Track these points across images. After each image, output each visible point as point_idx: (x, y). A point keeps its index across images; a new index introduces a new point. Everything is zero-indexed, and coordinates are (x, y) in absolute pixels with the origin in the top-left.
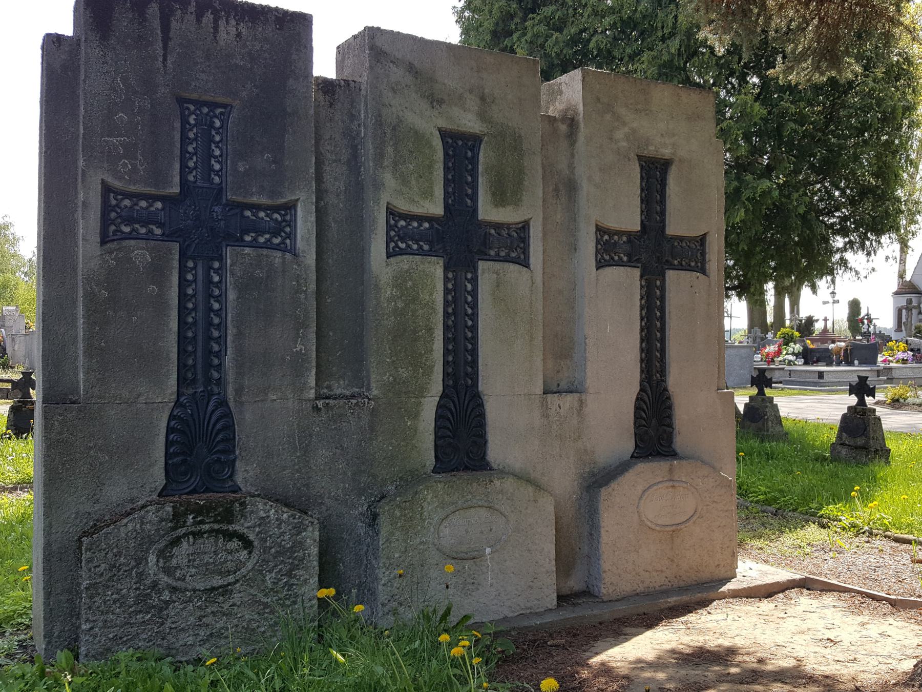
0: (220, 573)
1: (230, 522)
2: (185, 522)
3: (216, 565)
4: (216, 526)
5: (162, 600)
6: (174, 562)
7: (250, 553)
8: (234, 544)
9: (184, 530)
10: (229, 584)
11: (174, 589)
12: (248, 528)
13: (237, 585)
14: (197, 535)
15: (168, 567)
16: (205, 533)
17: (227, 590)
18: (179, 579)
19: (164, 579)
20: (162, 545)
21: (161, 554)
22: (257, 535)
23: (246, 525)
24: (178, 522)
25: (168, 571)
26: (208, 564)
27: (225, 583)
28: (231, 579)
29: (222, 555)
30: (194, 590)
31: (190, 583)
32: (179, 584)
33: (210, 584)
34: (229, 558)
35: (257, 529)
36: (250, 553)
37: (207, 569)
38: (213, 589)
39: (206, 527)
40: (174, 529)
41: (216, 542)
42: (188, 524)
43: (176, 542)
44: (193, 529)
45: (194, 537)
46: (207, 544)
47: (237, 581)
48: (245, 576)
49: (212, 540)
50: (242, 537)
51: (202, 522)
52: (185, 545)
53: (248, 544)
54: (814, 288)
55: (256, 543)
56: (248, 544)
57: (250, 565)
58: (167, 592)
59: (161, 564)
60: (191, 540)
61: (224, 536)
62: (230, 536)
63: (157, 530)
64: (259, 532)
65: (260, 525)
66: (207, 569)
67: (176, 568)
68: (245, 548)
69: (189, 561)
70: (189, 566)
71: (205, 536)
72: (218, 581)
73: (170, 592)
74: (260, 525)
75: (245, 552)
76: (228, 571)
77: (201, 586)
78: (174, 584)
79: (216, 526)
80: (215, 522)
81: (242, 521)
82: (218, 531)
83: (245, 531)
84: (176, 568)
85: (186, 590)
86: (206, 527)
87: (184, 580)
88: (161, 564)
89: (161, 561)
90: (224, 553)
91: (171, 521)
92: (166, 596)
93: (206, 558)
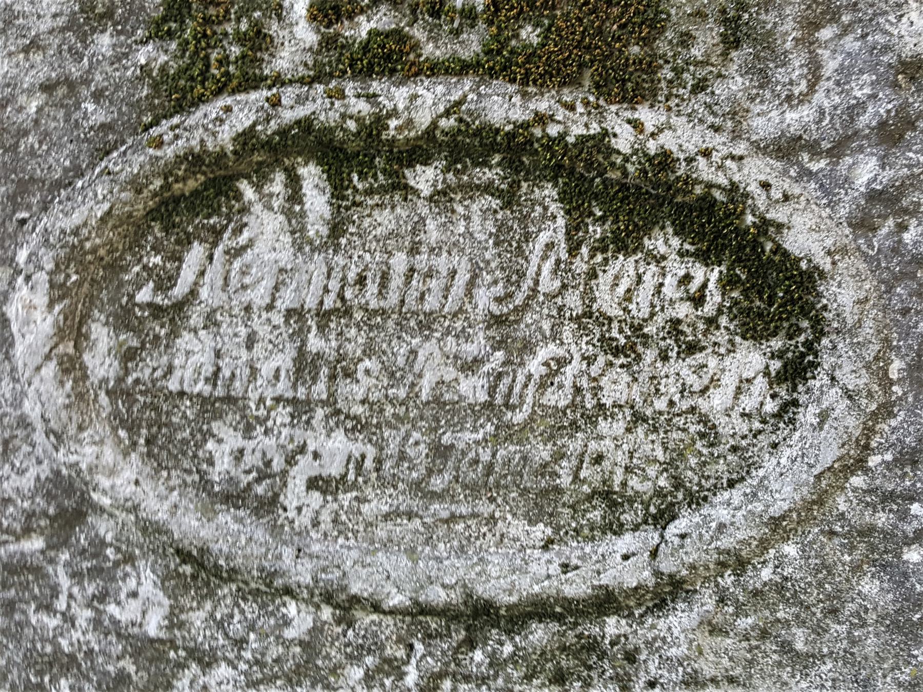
0: (542, 503)
1: (628, 85)
2: (258, 41)
3: (507, 433)
4: (502, 107)
5: (117, 629)
6: (191, 360)
7: (795, 371)
8: (663, 277)
9: (232, 117)
10: (606, 602)
11: (196, 571)
12: (786, 148)
13: (679, 621)
14: (362, 160)
15: (153, 389)
16: (418, 151)
17: (592, 646)
18: (233, 497)
19: (121, 479)
20: (86, 208)
21: (89, 281)
22: (863, 224)
23: (766, 122)
24: (206, 39)
25: (156, 425)
26: (443, 409)
27: (576, 587)
28: (622, 562)
29: (558, 359)
30: (346, 606)
31: (315, 544)
32: (228, 534)
33: (456, 570)
34: (617, 387)
35: (866, 171)
36: (795, 371)
37: (440, 452)
38: (479, 617)
39: (418, 104)
40: (180, 92)
41: (512, 241)
42: (284, 61)
43: (199, 199)
44: (316, 106)
45: (338, 189)
46: (444, 243)
47: (668, 592)
48: (738, 563)
49: (478, 217)
50: (719, 227)
51: (388, 58)
52: (265, 228)
53: (773, 295)
54: (359, 112)
55: (843, 295)
56: (773, 295)
57: (783, 480)
58: (145, 580)
59: (101, 363)
60: (317, 202)
61: (576, 201)
62: (638, 203)
63: (61, 90)
64: (885, 200)
65: (892, 135)
66: (440, 452)
67: (211, 408)
68: (754, 327)
69: (305, 366)
70: (301, 409)
71: (424, 178)
72: (517, 563)
73: (172, 583)
74: (892, 135)
75: (751, 360)
76: (607, 496)
77: (387, 576)
78: (190, 525)
79: (502, 107)
80: (498, 64)
81: (735, 85)
82: (518, 150)
83: (754, 172)
84: (211, 408)
85: (272, 589)
86: (418, 104)
87: (269, 505)
88: (101, 363)
89: (101, 335)
90: (573, 343)
91: (159, 32)
92: (142, 600)
93: (433, 367)
